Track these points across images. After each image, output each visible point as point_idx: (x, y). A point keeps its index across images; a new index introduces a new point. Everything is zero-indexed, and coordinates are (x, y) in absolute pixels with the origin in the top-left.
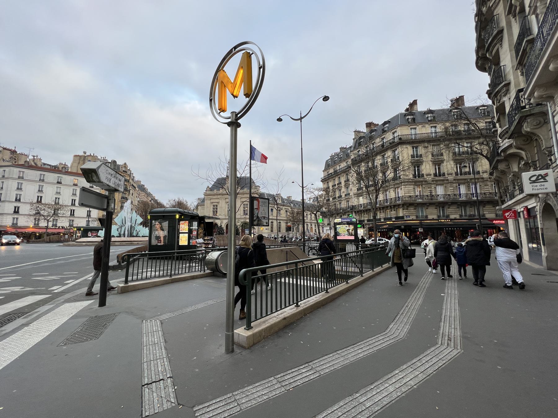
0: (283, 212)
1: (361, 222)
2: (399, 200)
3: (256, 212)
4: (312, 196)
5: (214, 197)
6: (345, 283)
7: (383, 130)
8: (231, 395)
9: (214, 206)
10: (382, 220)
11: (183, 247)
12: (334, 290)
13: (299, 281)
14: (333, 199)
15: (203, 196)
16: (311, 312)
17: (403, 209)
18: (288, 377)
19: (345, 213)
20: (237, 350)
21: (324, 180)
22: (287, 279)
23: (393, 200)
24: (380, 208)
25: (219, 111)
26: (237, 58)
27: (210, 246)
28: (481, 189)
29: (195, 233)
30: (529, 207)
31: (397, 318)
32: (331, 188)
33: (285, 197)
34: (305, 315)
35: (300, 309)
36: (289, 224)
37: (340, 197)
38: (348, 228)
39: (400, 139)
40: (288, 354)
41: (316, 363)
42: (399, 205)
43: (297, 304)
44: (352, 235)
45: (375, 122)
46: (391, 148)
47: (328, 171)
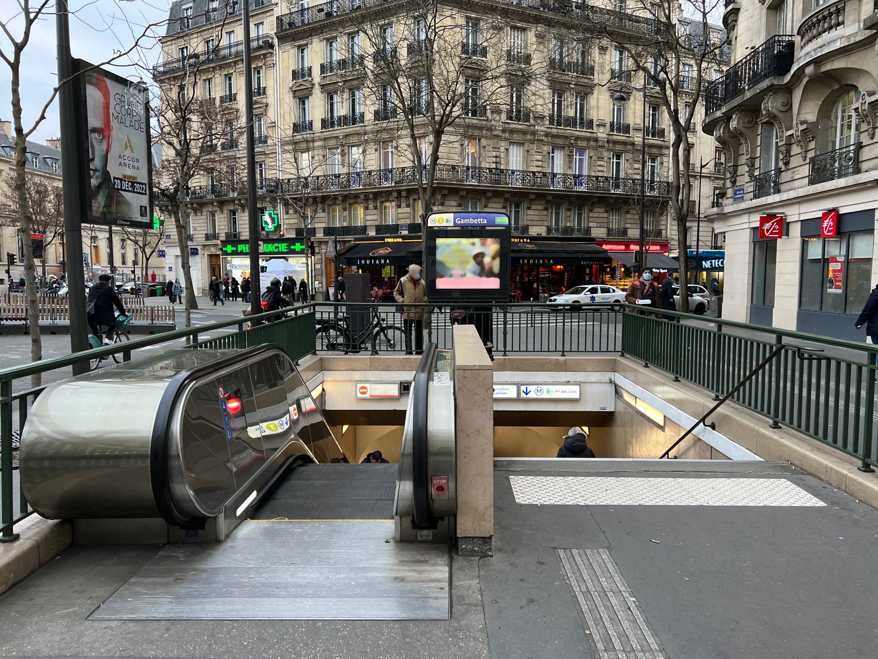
3: (97, 147)
10: (372, 233)
17: (367, 208)
28: (589, 169)
30: (842, 211)
38: (478, 249)
44: (490, 274)
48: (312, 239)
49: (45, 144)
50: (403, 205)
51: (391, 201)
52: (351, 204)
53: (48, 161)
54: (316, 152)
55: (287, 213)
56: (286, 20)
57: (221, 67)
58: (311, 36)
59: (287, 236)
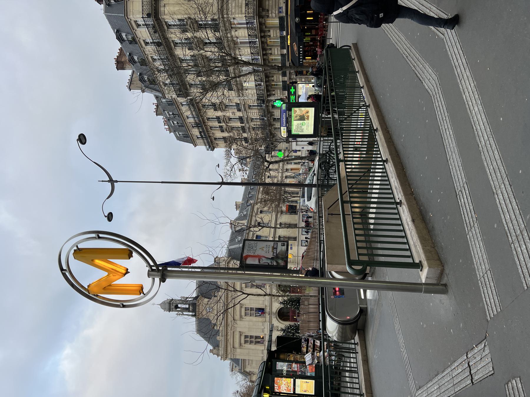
0: (266, 218)
2: (252, 23)
3: (264, 261)
4: (238, 166)
5: (230, 341)
6: (377, 134)
7: (131, 42)
8: (479, 282)
9: (246, 342)
10: (285, 51)
11: (318, 387)
12: (384, 152)
13: (373, 200)
14: (244, 132)
15: (228, 362)
16: (409, 185)
17: (271, 54)
18: (467, 219)
20: (443, 282)
21: (211, 145)
22: (371, 216)
23: (251, 32)
24: (264, 55)
25: (142, 295)
26: (78, 267)
27: (318, 343)
29: (295, 366)
31: (419, 75)
32: (226, 134)
33: (235, 214)
34: (412, 193)
35: (404, 201)
36: (284, 209)
37: (241, 119)
39: (149, 15)
40: (449, 217)
42: (261, 24)
43: (397, 203)
45: (116, 54)
47: (195, 138)
48: (288, 83)
50: (269, 34)
51: (267, 40)
52: (266, 27)
53: (250, 196)
55: (274, 94)
56: (178, 93)
57: (204, 123)
58: (167, 39)
59: (287, 95)
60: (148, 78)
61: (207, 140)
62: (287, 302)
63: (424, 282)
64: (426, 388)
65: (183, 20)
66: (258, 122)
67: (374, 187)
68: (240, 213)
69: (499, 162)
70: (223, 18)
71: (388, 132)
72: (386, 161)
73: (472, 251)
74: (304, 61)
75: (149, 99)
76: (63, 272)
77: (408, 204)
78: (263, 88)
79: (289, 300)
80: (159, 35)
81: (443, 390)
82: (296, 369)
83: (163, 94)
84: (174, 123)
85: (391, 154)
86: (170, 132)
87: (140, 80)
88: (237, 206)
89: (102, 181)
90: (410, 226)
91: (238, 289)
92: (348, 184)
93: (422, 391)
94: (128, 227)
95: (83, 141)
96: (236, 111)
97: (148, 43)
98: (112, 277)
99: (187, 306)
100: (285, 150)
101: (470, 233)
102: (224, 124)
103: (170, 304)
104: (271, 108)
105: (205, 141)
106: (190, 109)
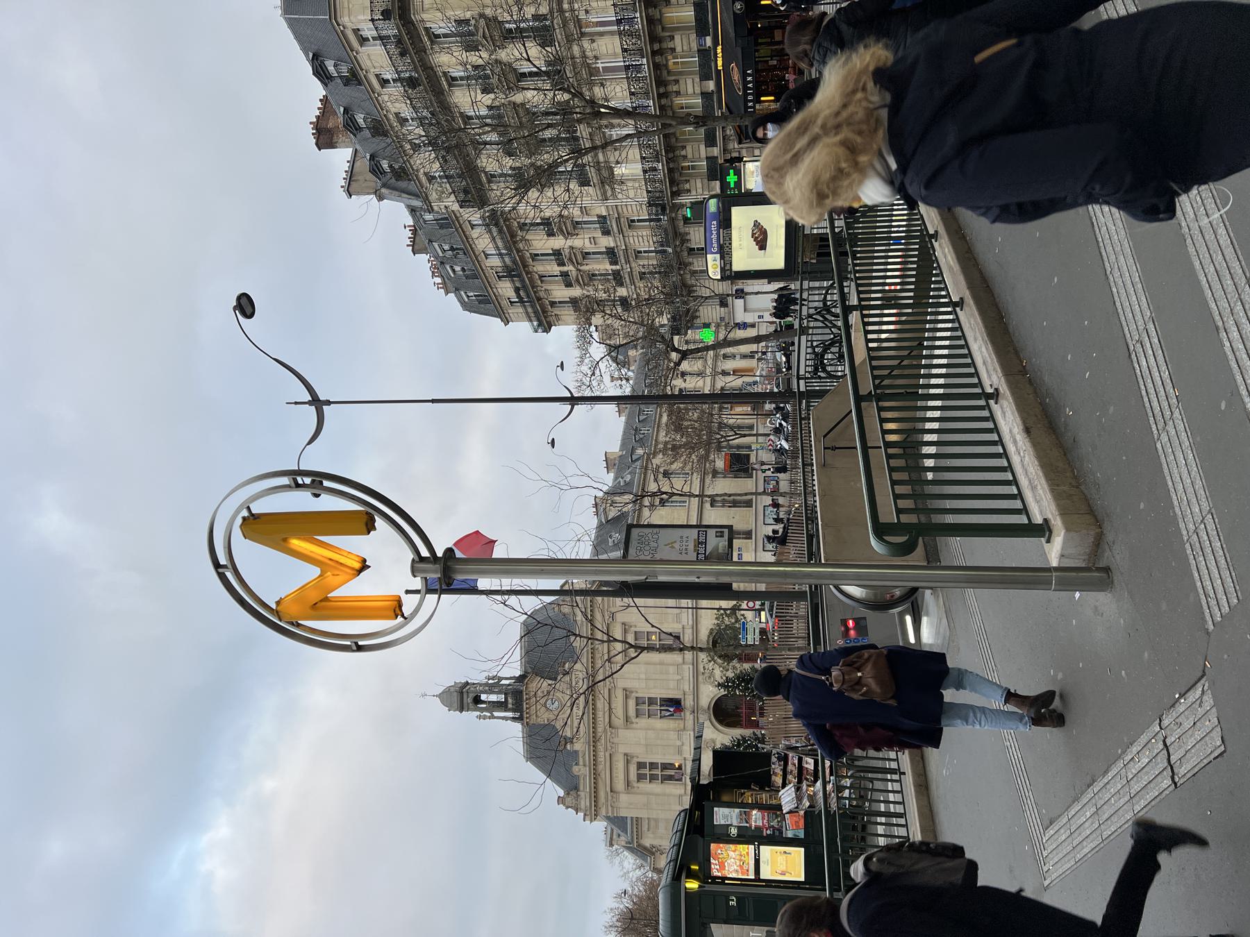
1: (716, 171)
2: (631, 21)
6: (936, 245)
7: (347, 82)
9: (640, 777)
10: (711, 85)
11: (812, 864)
12: (956, 284)
15: (600, 825)
16: (1017, 353)
17: (678, 93)
18: (1155, 404)
19: (676, 234)
21: (544, 322)
23: (629, 43)
24: (660, 96)
25: (400, 619)
26: (254, 559)
27: (809, 763)
32: (576, 292)
34: (1024, 371)
35: (1004, 389)
36: (720, 464)
37: (611, 254)
39: (386, 14)
41: (1132, 332)
42: (651, 21)
43: (989, 397)
44: (763, 604)
46: (421, 51)
47: (505, 303)
48: (721, 161)
49: (623, 419)
50: (671, 45)
52: (663, 29)
53: (642, 418)
54: (612, 159)
55: (689, 191)
57: (525, 266)
58: (432, 68)
60: (390, 166)
61: (533, 307)
62: (734, 682)
63: (1054, 564)
64: (1065, 820)
65: (467, 22)
66: (652, 258)
67: (933, 381)
68: (616, 478)
69: (1229, 252)
70: (561, 11)
71: (963, 237)
72: (960, 304)
73: (1168, 478)
74: (757, 106)
75: (394, 214)
76: (220, 570)
77: (1013, 394)
78: (660, 176)
79: (738, 677)
80: (413, 61)
81: (1106, 816)
82: (760, 823)
83: (426, 199)
84: (454, 271)
85: (971, 286)
86: (447, 293)
87: (373, 171)
88: (609, 463)
89: (296, 403)
90: (1020, 444)
91: (618, 636)
92: (874, 378)
93: (1056, 828)
94: (362, 453)
95: (249, 312)
96: (598, 234)
97: (387, 81)
98: (330, 579)
99: (502, 698)
100: (718, 326)
101: (1164, 438)
102: (571, 268)
103: (462, 693)
104: (686, 254)
105: (530, 310)
106: (490, 231)
